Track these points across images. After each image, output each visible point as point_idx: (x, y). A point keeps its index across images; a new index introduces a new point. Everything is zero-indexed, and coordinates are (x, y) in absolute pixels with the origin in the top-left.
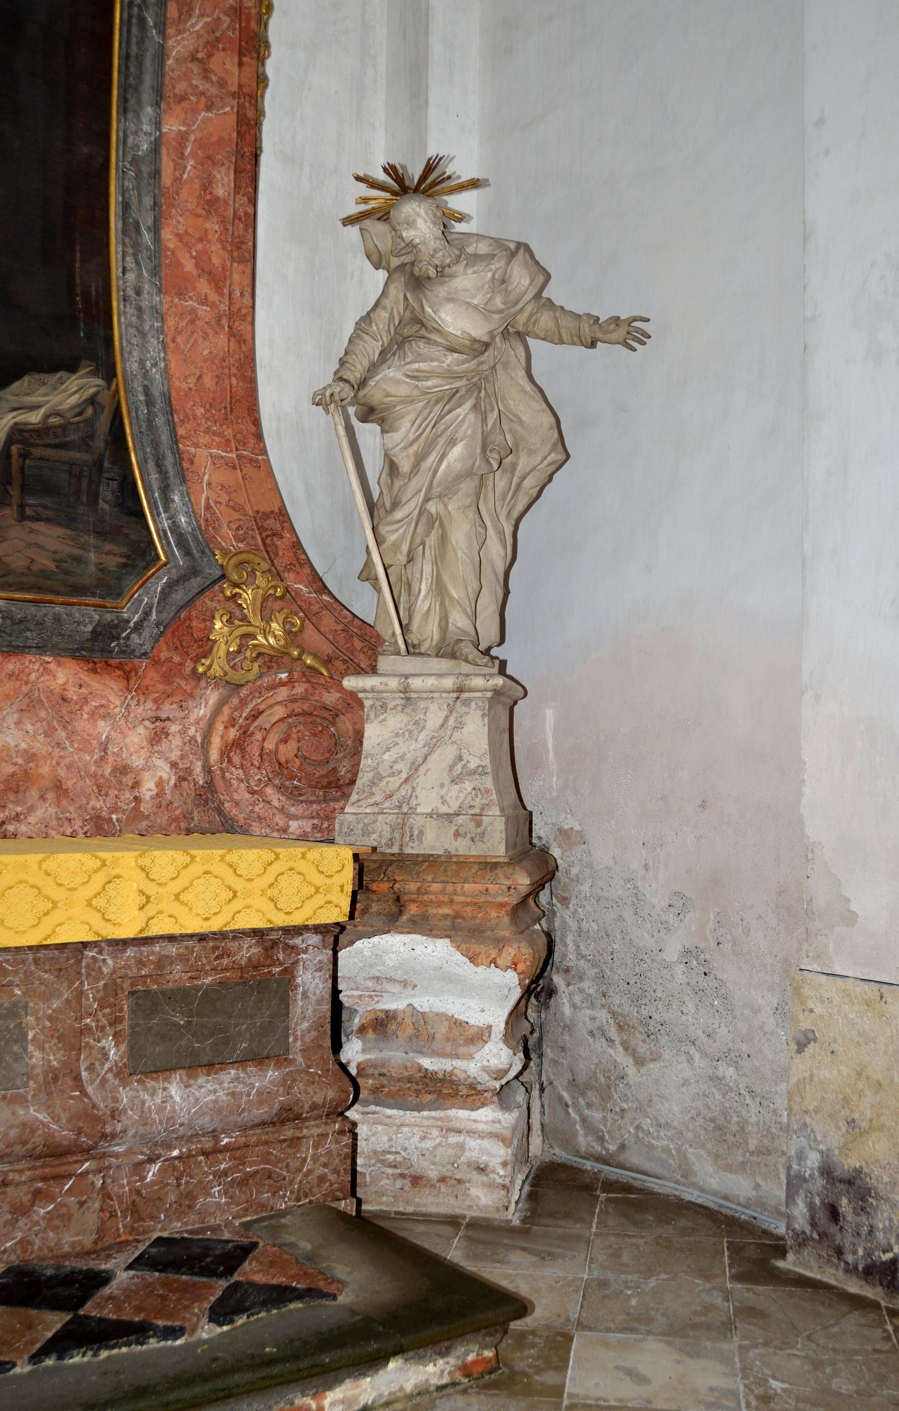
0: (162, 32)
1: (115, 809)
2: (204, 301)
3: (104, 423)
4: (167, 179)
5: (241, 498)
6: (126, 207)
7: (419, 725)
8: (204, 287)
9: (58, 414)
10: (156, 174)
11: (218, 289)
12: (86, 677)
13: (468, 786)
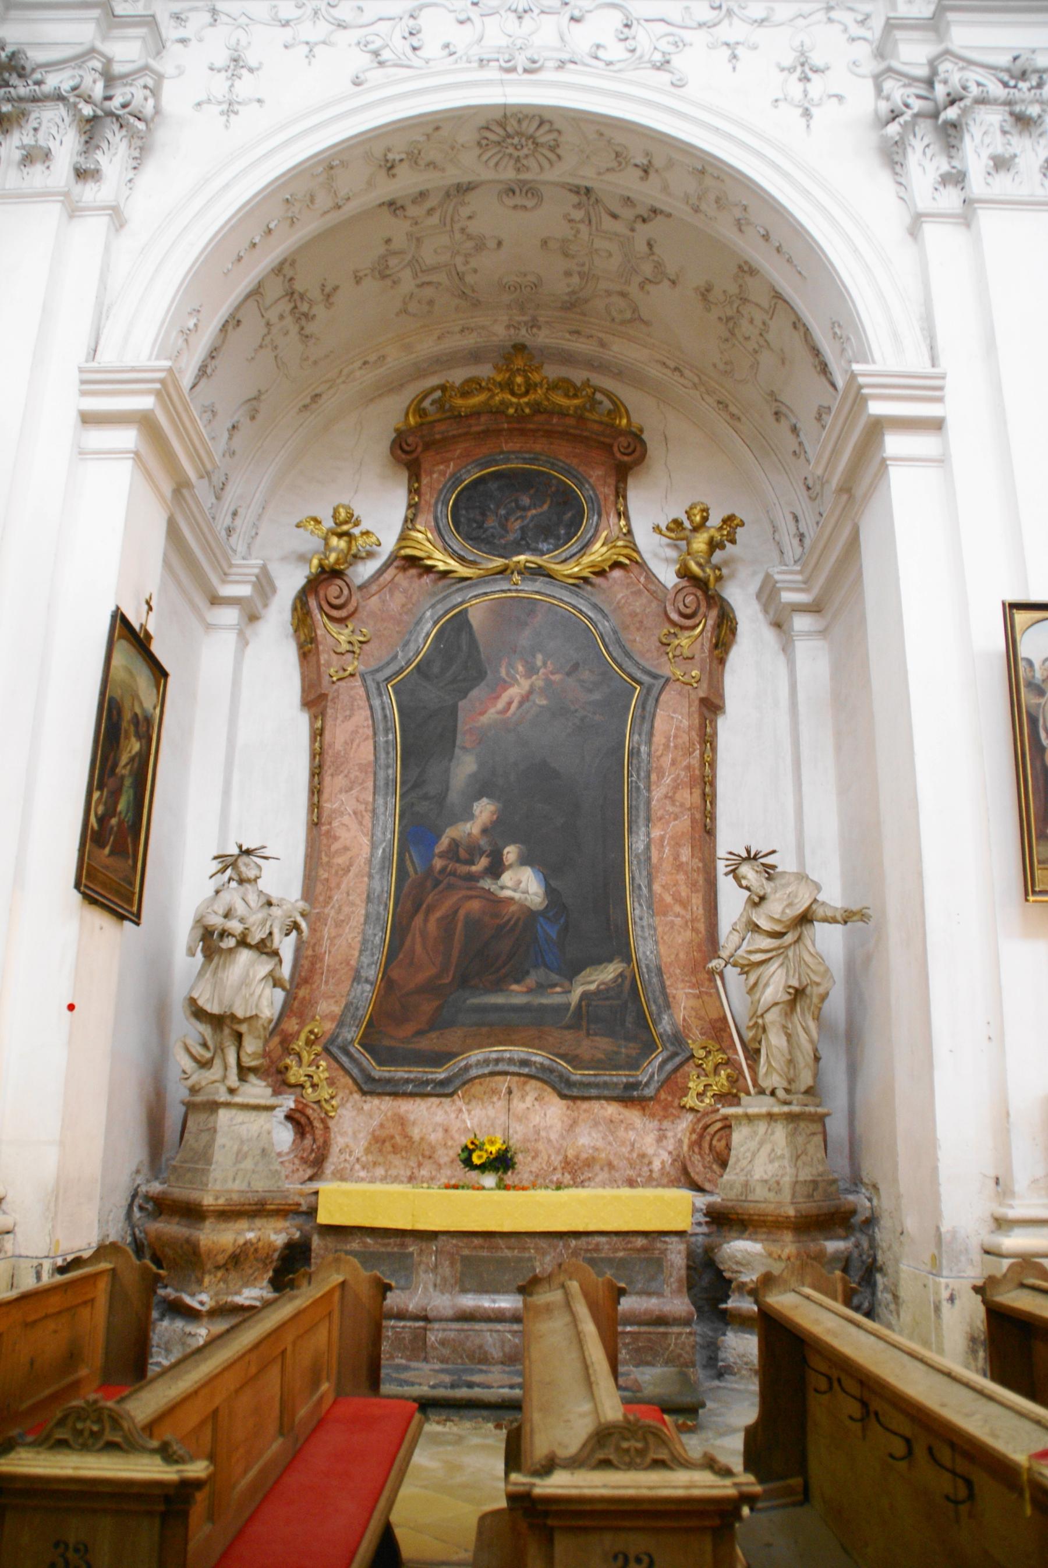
0: (649, 790)
1: (639, 1175)
2: (678, 915)
3: (627, 983)
4: (654, 860)
5: (702, 1013)
6: (633, 879)
7: (755, 1133)
8: (677, 908)
9: (603, 983)
10: (649, 858)
11: (685, 907)
12: (622, 1109)
13: (776, 1164)
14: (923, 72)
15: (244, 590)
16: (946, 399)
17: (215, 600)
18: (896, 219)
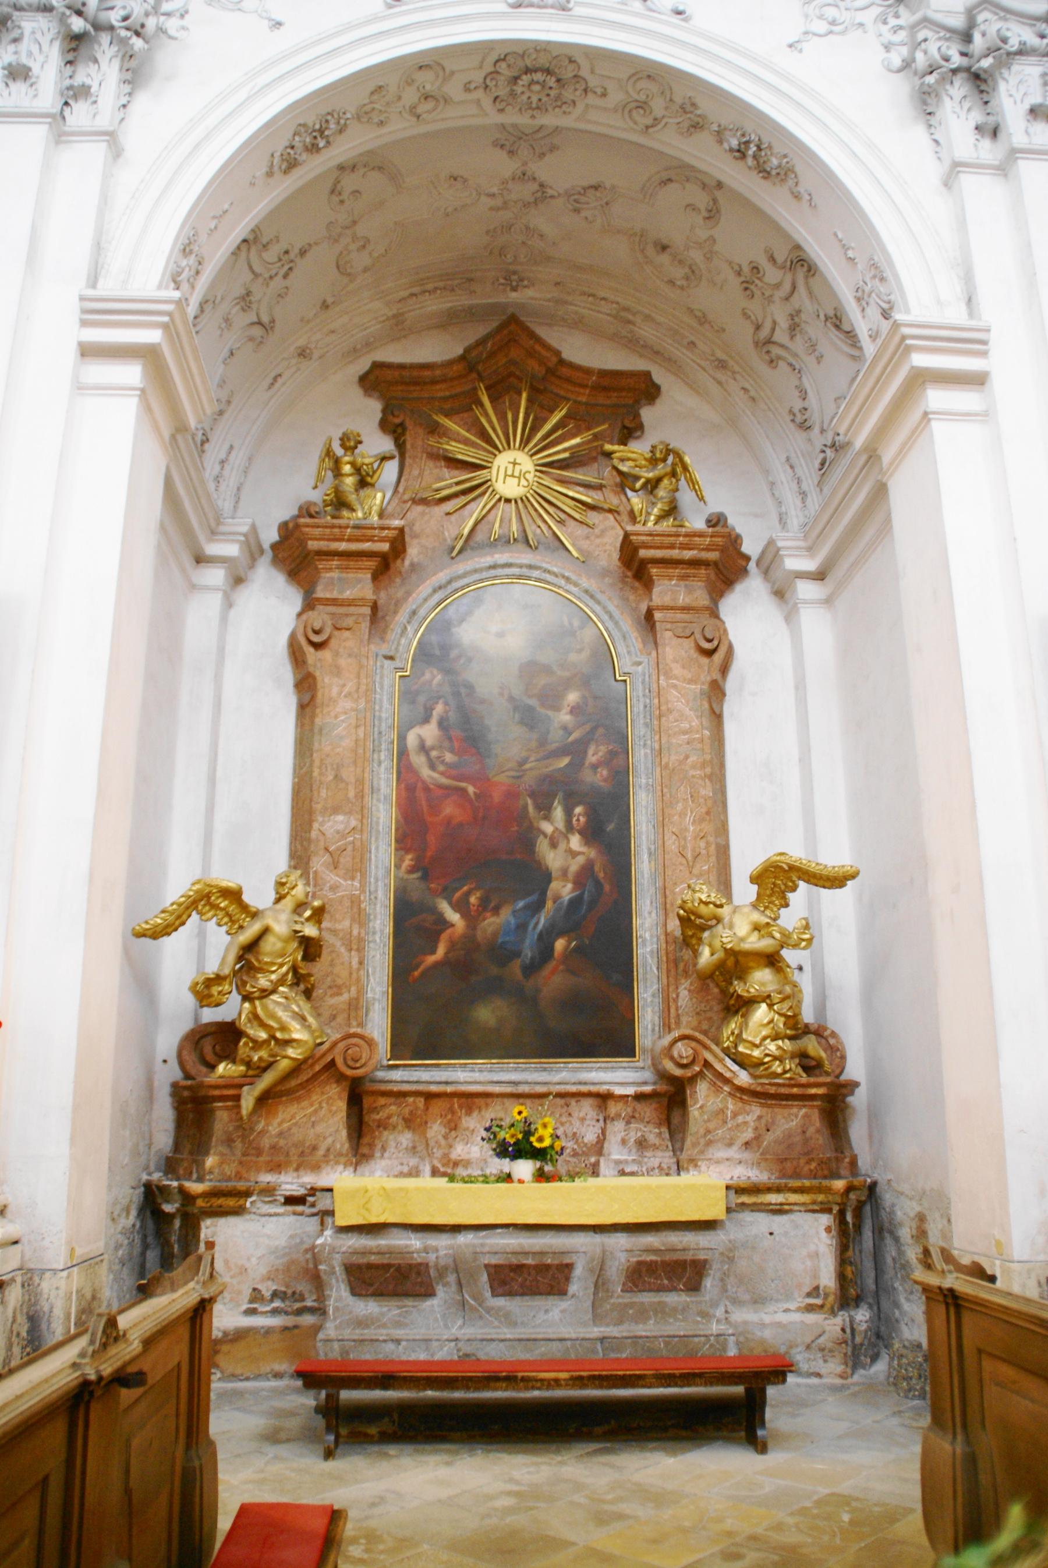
14: (958, 22)
15: (231, 550)
16: (991, 353)
17: (200, 559)
18: (934, 171)
